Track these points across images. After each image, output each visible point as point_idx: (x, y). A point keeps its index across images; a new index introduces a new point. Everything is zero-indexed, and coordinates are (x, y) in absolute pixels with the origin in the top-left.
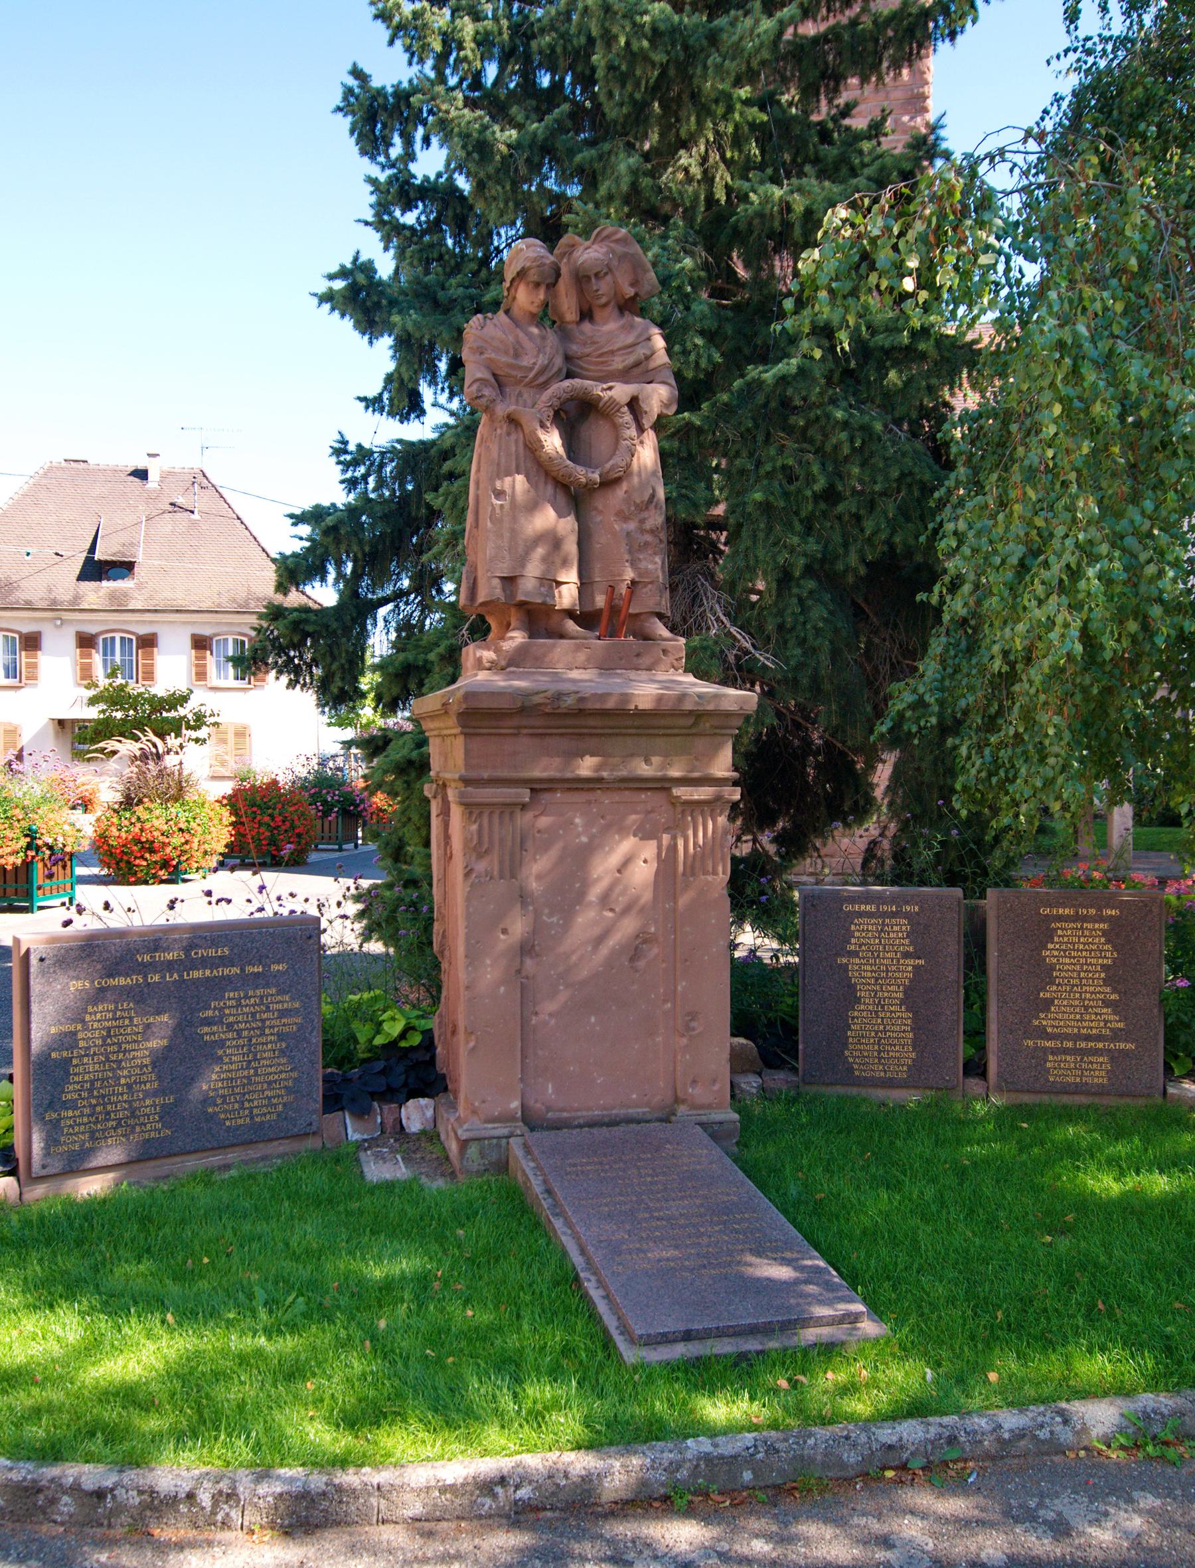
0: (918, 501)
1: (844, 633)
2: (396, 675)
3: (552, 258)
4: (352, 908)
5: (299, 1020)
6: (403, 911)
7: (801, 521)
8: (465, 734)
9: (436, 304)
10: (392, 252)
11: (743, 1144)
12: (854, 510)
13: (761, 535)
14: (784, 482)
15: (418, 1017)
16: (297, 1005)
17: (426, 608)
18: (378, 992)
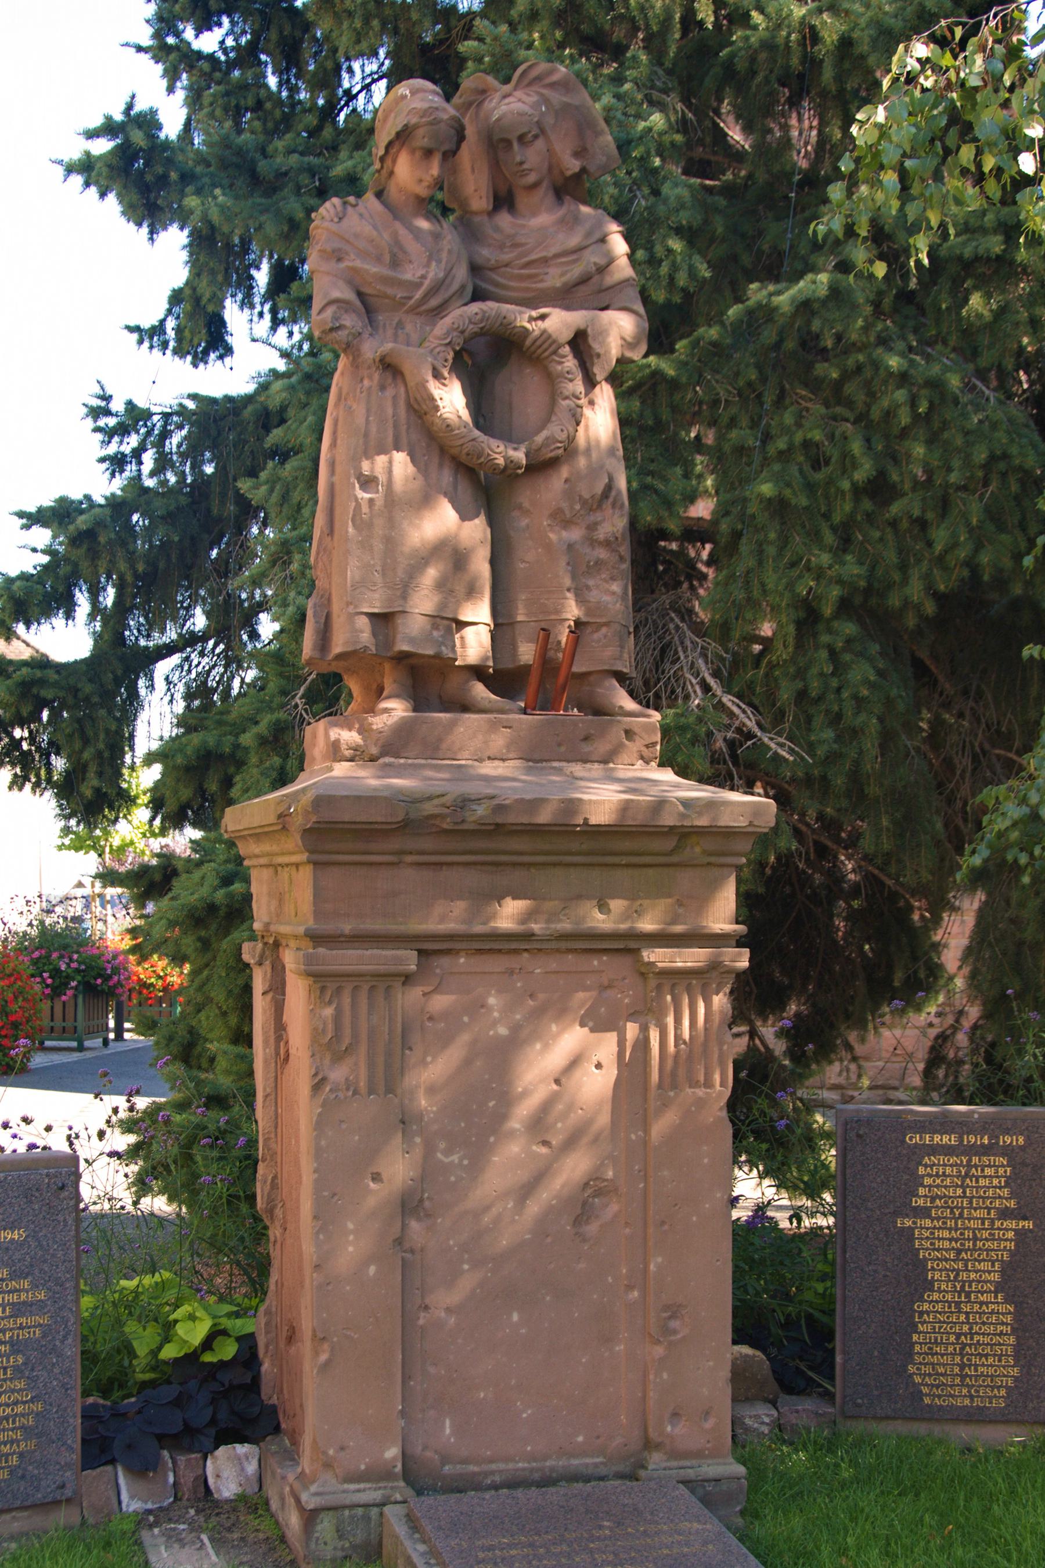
0: (1017, 498)
1: (901, 707)
2: (188, 769)
3: (449, 111)
4: (122, 1141)
5: (43, 1320)
6: (207, 1148)
7: (834, 529)
8: (316, 864)
9: (255, 179)
10: (180, 95)
11: (751, 1513)
12: (916, 513)
13: (771, 550)
14: (807, 468)
15: (229, 1315)
16: (42, 1296)
17: (233, 661)
18: (166, 1275)
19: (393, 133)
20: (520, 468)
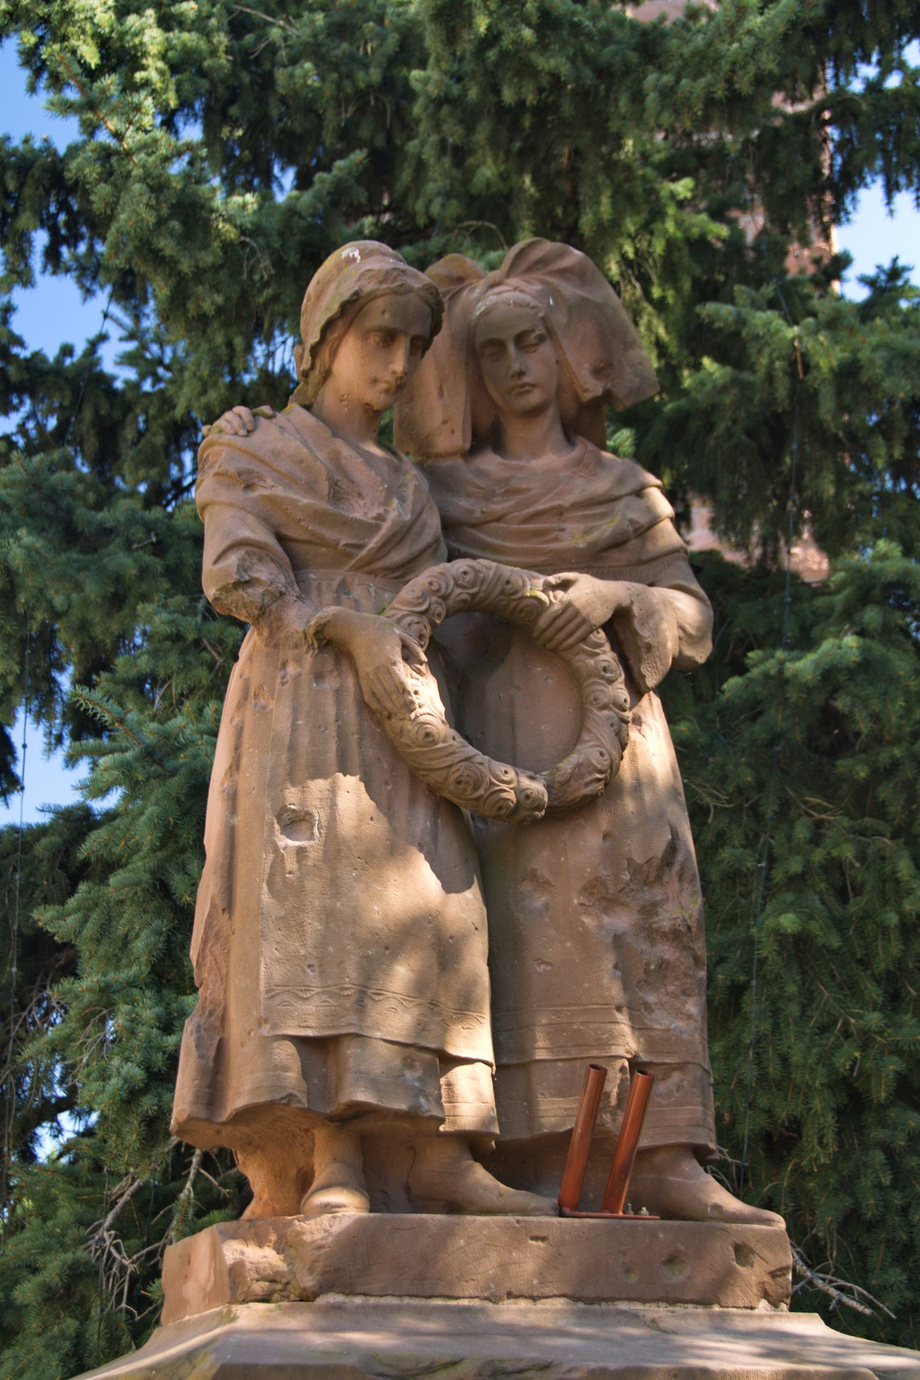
7: (877, 980)
13: (794, 1009)
14: (832, 900)
19: (335, 307)
20: (538, 808)
